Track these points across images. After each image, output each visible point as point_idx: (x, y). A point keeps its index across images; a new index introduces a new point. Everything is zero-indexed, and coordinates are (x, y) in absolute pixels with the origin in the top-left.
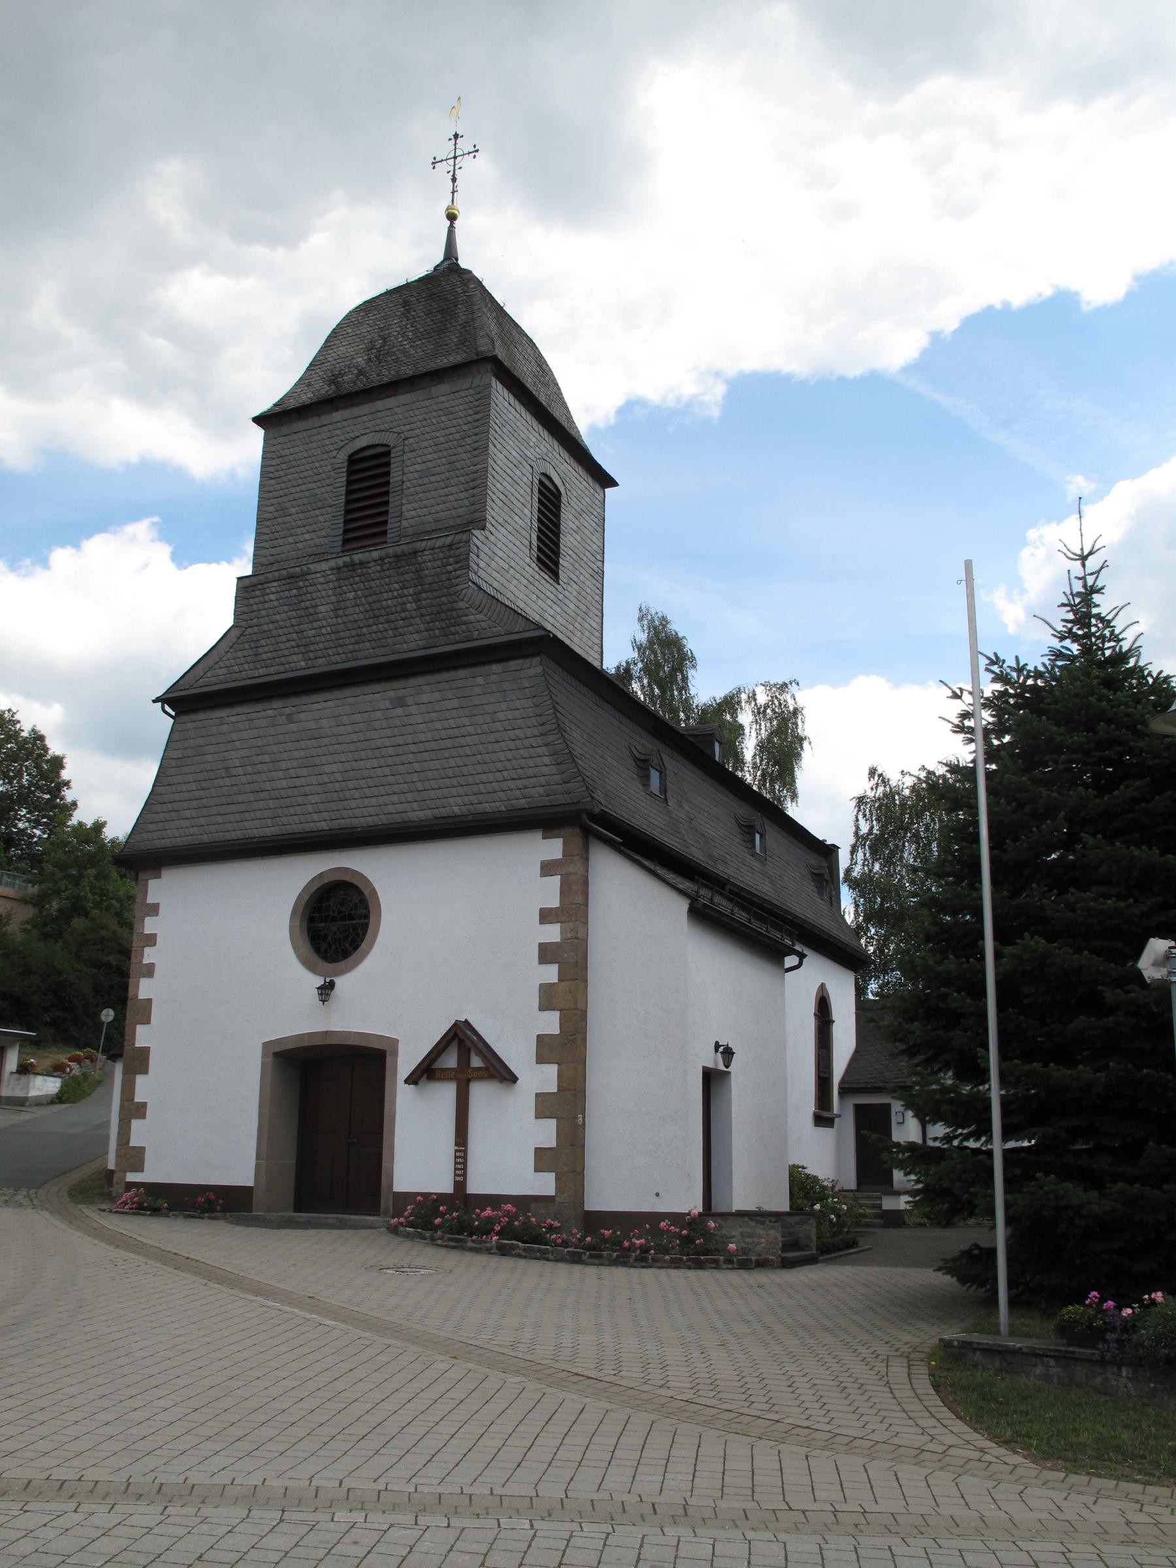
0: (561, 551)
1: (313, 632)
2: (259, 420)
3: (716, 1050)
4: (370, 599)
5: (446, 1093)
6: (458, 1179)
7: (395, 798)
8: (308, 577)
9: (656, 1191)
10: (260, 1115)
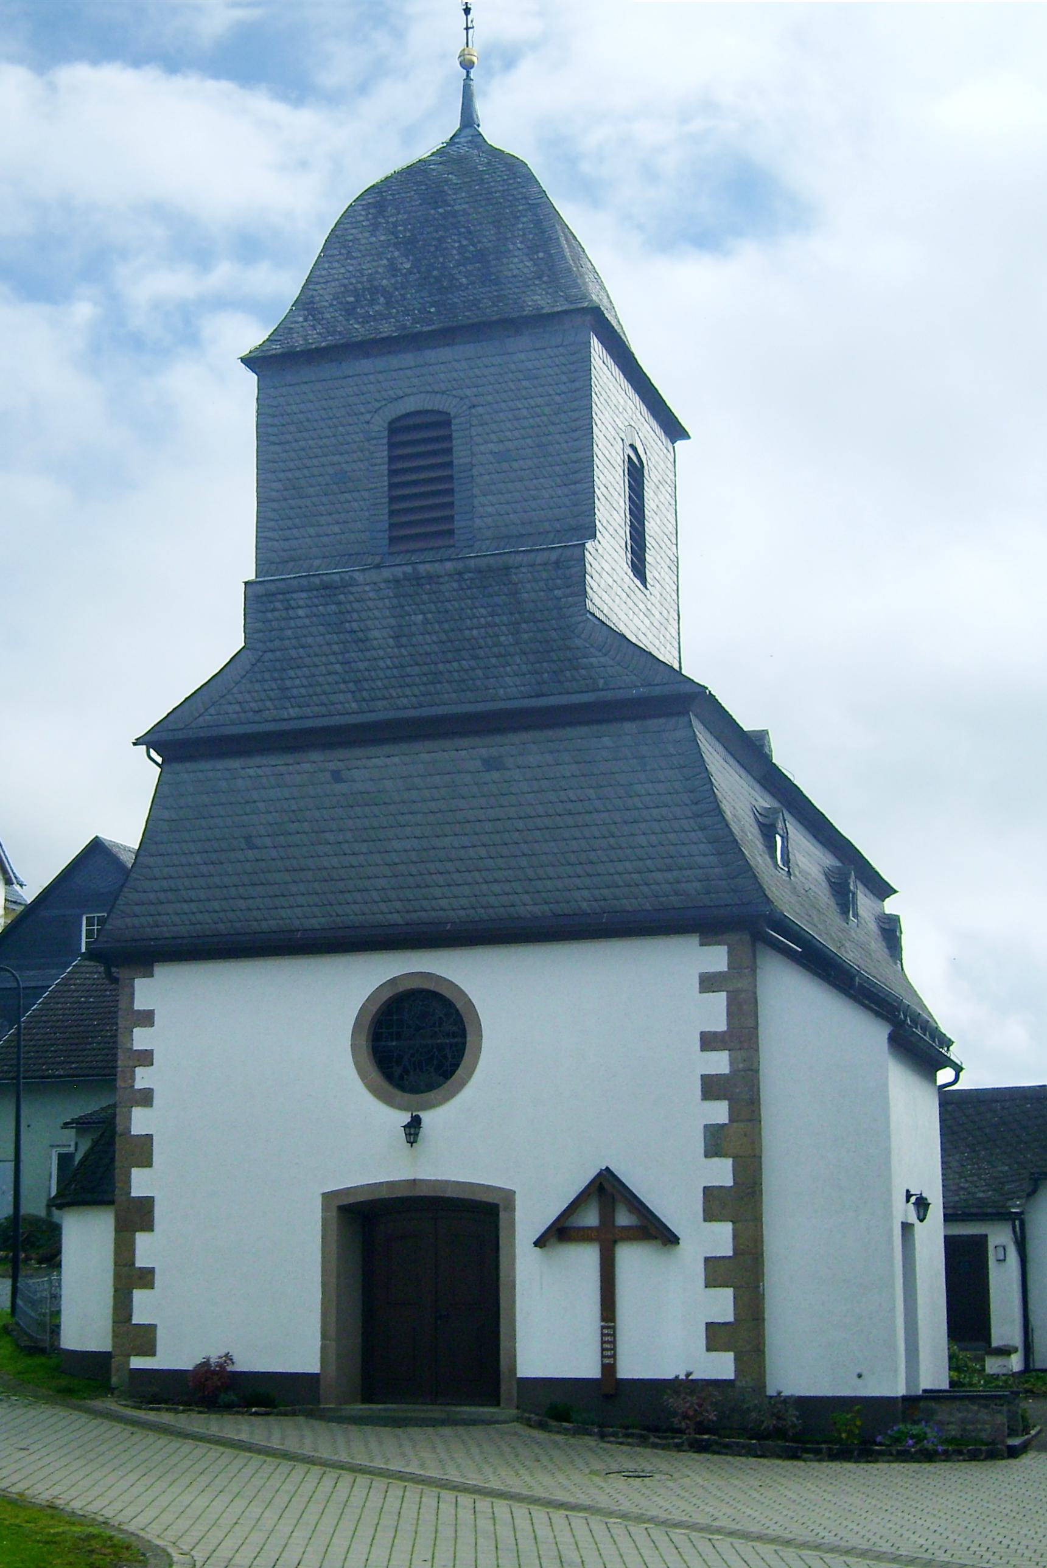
0: (647, 544)
1: (366, 664)
2: (249, 361)
3: (908, 1201)
4: (446, 626)
5: (587, 1257)
6: (607, 1361)
7: (496, 888)
8: (354, 589)
9: (859, 1371)
10: (324, 1285)
